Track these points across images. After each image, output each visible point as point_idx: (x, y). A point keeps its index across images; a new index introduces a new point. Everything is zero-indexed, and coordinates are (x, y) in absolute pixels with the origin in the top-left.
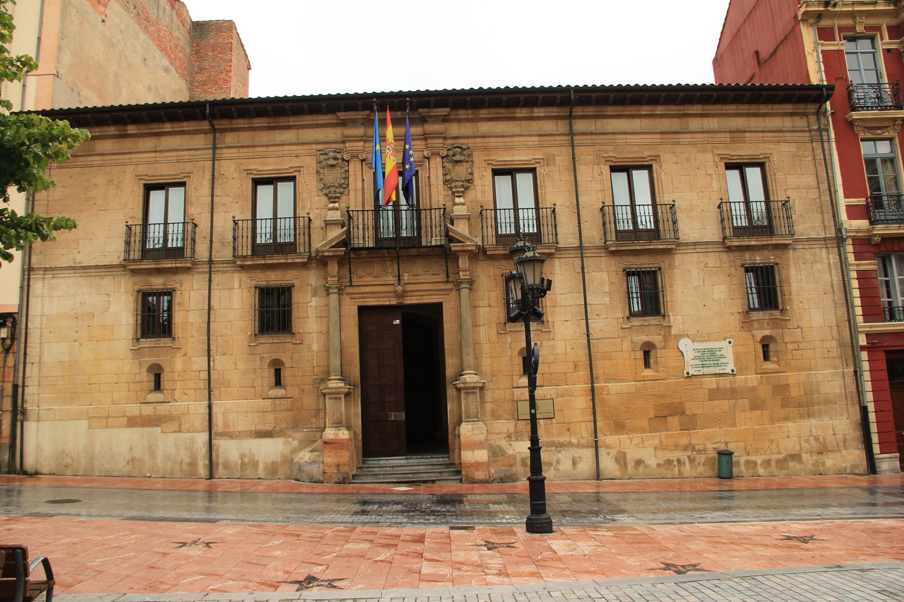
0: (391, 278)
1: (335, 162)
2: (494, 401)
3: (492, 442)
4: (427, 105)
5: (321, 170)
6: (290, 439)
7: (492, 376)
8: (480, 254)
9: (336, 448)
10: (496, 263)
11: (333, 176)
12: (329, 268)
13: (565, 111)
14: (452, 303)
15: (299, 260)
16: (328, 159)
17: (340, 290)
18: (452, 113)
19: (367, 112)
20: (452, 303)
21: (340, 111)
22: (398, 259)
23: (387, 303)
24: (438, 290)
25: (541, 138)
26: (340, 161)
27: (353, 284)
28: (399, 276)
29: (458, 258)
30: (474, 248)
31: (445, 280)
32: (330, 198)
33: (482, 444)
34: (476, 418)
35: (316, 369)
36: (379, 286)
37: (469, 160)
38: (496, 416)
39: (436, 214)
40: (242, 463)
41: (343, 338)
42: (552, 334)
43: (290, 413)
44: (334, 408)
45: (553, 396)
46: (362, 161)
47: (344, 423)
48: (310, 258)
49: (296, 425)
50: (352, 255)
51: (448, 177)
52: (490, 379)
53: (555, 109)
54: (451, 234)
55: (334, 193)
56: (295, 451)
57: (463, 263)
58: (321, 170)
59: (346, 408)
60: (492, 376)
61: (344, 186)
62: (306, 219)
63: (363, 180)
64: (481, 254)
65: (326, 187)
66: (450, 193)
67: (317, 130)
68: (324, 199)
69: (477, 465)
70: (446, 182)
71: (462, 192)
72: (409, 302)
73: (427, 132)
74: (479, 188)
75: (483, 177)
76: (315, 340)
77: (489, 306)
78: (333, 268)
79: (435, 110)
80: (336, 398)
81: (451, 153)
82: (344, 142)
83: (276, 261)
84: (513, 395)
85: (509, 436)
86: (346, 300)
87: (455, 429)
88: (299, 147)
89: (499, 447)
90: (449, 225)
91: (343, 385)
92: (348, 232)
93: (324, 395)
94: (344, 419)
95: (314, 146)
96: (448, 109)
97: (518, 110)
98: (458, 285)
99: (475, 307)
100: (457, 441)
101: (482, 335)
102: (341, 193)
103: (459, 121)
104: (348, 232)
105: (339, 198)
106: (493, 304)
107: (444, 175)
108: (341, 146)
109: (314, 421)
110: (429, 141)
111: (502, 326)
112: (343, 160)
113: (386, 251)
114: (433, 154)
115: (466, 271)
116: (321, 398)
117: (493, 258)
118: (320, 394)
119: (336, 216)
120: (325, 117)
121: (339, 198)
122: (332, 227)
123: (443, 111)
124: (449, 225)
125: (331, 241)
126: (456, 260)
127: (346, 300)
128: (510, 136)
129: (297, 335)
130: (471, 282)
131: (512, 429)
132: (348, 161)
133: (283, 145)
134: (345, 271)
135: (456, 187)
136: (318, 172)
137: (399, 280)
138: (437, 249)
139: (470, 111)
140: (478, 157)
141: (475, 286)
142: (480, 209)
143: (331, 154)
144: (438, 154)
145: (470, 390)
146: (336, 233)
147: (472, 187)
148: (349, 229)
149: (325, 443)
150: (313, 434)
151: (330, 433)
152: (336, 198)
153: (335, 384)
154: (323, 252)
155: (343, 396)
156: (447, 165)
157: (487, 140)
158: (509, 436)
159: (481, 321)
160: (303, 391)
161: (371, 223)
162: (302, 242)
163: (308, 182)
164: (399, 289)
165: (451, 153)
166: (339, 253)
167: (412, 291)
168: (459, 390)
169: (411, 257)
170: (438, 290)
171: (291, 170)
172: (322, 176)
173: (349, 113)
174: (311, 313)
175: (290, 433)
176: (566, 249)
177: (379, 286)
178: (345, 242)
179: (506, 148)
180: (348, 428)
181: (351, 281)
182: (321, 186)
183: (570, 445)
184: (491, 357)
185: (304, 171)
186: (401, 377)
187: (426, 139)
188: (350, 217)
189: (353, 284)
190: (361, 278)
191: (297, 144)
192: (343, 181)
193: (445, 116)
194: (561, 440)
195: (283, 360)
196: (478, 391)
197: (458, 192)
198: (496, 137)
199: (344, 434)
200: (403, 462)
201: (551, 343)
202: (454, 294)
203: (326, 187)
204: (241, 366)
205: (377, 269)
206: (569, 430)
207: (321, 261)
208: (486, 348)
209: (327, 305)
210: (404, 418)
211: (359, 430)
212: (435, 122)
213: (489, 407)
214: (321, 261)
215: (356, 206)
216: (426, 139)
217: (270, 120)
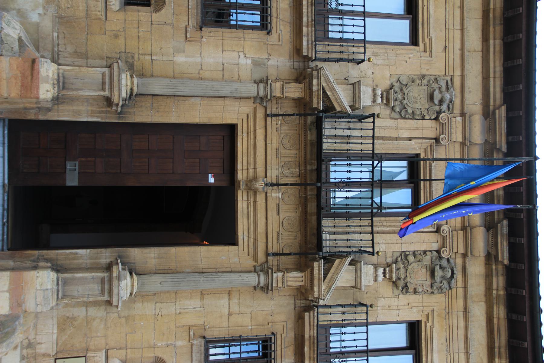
0: (275, 173)
1: (436, 102)
2: (88, 321)
3: (22, 320)
4: (513, 233)
5: (425, 82)
6: (41, 11)
7: (127, 318)
8: (306, 302)
9: (24, 76)
10: (290, 325)
11: (417, 97)
12: (294, 85)
14: (236, 260)
15: (305, 43)
16: (441, 92)
17: (261, 98)
18: (500, 267)
19: (504, 149)
20: (236, 260)
21: (508, 110)
22: (303, 185)
23: (239, 167)
24: (255, 239)
26: (437, 108)
27: (269, 119)
28: (278, 185)
29: (301, 271)
30: (316, 295)
31: (270, 251)
32: (387, 91)
33: (19, 305)
34: (62, 293)
35: (148, 58)
36: (265, 155)
37: (434, 288)
38: (64, 324)
39: (361, 240)
41: (193, 99)
43: (82, 14)
44: (89, 79)
46: (437, 140)
47: (65, 92)
48: (307, 59)
49: (63, 20)
50: (310, 119)
51: (411, 258)
52: (122, 314)
54: (337, 261)
55: (393, 97)
56: (22, 15)
57: (295, 278)
58: (425, 82)
59: (87, 99)
60: (127, 318)
61: (403, 113)
62: (362, 57)
63: (410, 139)
64: (303, 303)
65: (403, 86)
66: (389, 260)
67: (480, 78)
68: (386, 84)
70: (404, 255)
71: (391, 278)
72: (240, 198)
73: (474, 230)
74: (394, 301)
75: (411, 308)
76: (190, 60)
77: (230, 314)
78: (294, 91)
79: (505, 244)
80: (104, 83)
81: (444, 263)
82: (463, 114)
83: (305, 10)
84: (98, 350)
85: (30, 345)
86: (246, 108)
87: (47, 260)
88: (458, 52)
89: (14, 331)
90: (349, 259)
91: (124, 95)
92: (343, 115)
93: (110, 67)
94: (71, 93)
95: (458, 73)
96: (506, 262)
98: (263, 269)
99: (229, 293)
100: (28, 264)
101: (188, 302)
102: (393, 109)
103: (488, 276)
104: (343, 115)
105: (387, 104)
106: (233, 319)
107: (414, 253)
108: (457, 111)
109: (70, 49)
110: (461, 233)
111: (201, 332)
112: (439, 113)
113: (315, 167)
114: (444, 238)
115: (284, 282)
116: (104, 63)
117: (299, 319)
118: (110, 62)
119: (366, 99)
120: (498, 89)
121: (387, 104)
122: (351, 92)
124: (349, 259)
125: (333, 90)
126: (299, 268)
127: (246, 108)
128: (467, 348)
129: (198, 34)
130: (267, 288)
132: (436, 119)
133: (462, 29)
134: (288, 108)
135: (398, 269)
136: (423, 77)
137: (272, 185)
138: (315, 241)
139: (502, 293)
140: (437, 301)
141: (258, 293)
142: (369, 304)
143: (447, 96)
144: (443, 246)
145: (108, 286)
146: (342, 97)
147: (397, 292)
148: (348, 116)
149: (34, 61)
150: (49, 46)
151: (48, 70)
152: (388, 100)
153: (126, 83)
154: (318, 78)
155: (107, 93)
156: (428, 257)
157: (461, 314)
158: (30, 345)
159: (208, 300)
160: (116, 36)
161: (355, 147)
162: (329, 48)
163: (411, 63)
164: (260, 185)
165: (444, 263)
166: (315, 99)
167: (255, 202)
168: (109, 268)
169: (304, 203)
170: (255, 239)
171: (427, 40)
172: (418, 82)
173: (504, 124)
174: (230, 57)
175: (52, 10)
177: (265, 155)
178: (329, 109)
179: (449, 342)
180: (57, 100)
181: (273, 115)
182: (404, 81)
184: (156, 316)
185: (425, 57)
186: (131, 182)
187: (464, 228)
188: (361, 118)
189: (269, 119)
190: (278, 130)
191: (462, 49)
192: (410, 111)
193: (496, 257)
195: (163, 11)
196: (106, 297)
197: (391, 271)
198: (466, 328)
199: (46, 92)
202: (249, 263)
203: (403, 86)
205: (290, 154)
207: (303, 75)
208: (169, 309)
209: (239, 80)
210: (69, 183)
211: (53, 116)
212: (487, 243)
213: (80, 312)
214: (303, 75)
215: (380, 128)
216: (464, 228)
217: (499, 12)
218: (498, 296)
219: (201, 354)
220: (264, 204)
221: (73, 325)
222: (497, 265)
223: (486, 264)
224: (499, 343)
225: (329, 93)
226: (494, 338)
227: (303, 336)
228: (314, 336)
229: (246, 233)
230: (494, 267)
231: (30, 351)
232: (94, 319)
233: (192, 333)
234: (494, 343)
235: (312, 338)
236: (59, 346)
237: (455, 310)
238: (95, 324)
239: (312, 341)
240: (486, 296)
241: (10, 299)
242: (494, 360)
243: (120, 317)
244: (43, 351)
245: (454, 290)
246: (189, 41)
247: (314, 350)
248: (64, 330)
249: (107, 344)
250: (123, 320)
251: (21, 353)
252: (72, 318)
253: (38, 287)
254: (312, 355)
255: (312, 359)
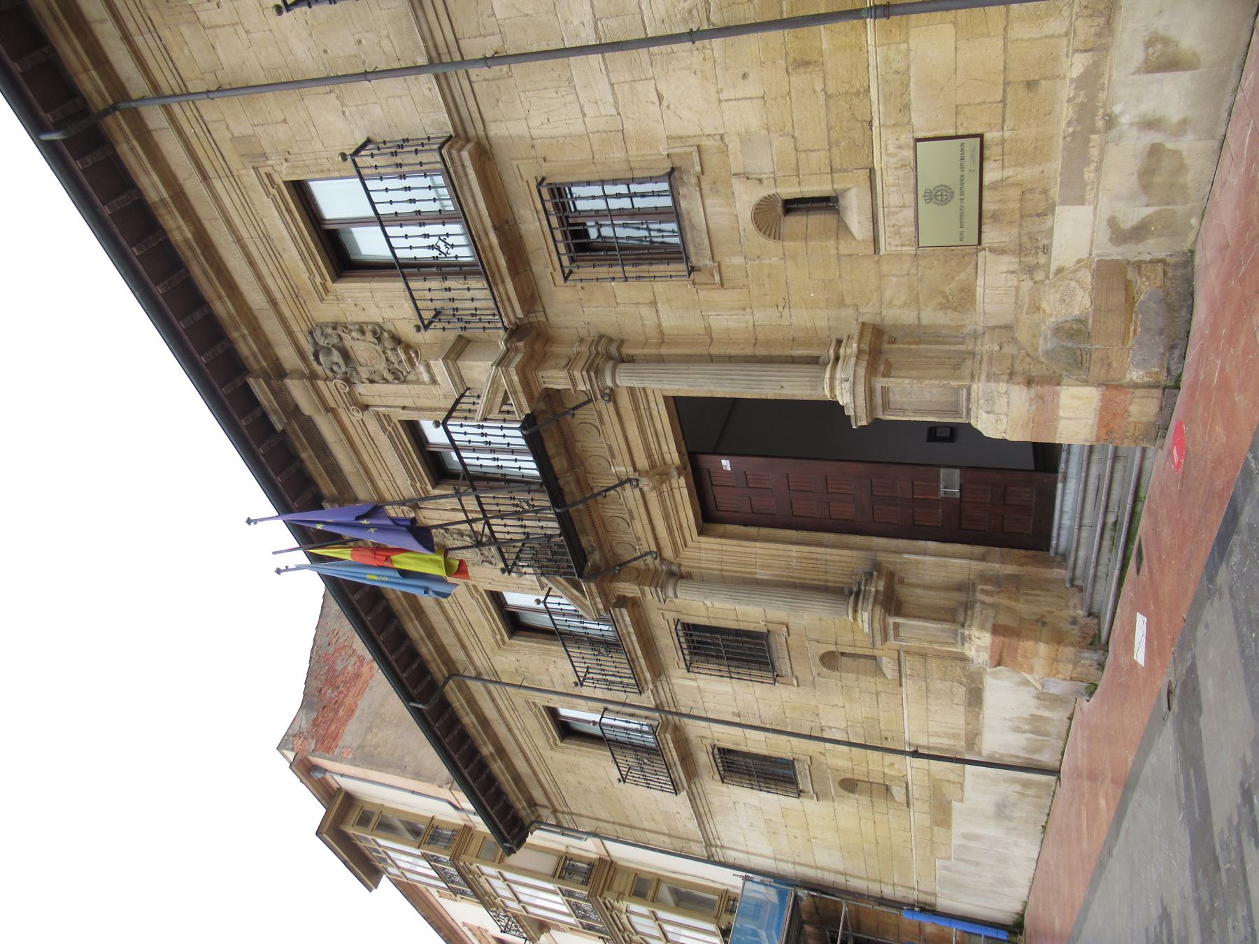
7: (842, 304)
13: (117, 126)
18: (256, 366)
25: (211, 173)
36: (654, 514)
40: (1032, 732)
42: (706, 143)
45: (907, 138)
50: (596, 557)
52: (851, 311)
53: (123, 149)
60: (842, 304)
69: (1108, 417)
72: (676, 456)
84: (898, 257)
96: (251, 381)
97: (176, 237)
101: (733, 325)
103: (266, 346)
107: (387, 381)
123: (259, 388)
131: (1007, 262)
157: (278, 295)
158: (1031, 270)
167: (649, 456)
176: (453, 108)
179: (276, 255)
183: (1091, 81)
194: (1066, 112)
200: (1072, 485)
201: (734, 145)
204: (838, 700)
206: (1031, 85)
213: (932, 316)
218: (237, 328)
219: (694, 240)
220: (636, 454)
221: (946, 297)
222: (262, 367)
223: (278, 359)
224: (199, 263)
225: (574, 591)
226: (211, 266)
227: (514, 272)
228: (496, 285)
229: (655, 413)
230: (264, 364)
231: (1030, 260)
232: (905, 305)
233: (717, 278)
234: (207, 260)
235: (499, 281)
236: (973, 263)
237: (290, 301)
238: (903, 297)
239: (497, 277)
240: (255, 318)
241: (1058, 407)
242: (193, 234)
243: (856, 306)
244: (1005, 259)
245: (305, 328)
246: (782, 623)
247: (488, 263)
248: (962, 290)
249: (877, 262)
250: (848, 302)
251: (1049, 258)
252: (946, 308)
253: (1004, 419)
254: (490, 255)
255: (488, 249)
